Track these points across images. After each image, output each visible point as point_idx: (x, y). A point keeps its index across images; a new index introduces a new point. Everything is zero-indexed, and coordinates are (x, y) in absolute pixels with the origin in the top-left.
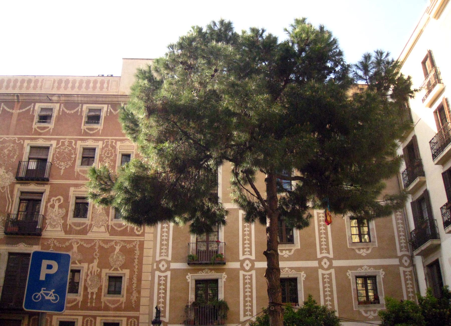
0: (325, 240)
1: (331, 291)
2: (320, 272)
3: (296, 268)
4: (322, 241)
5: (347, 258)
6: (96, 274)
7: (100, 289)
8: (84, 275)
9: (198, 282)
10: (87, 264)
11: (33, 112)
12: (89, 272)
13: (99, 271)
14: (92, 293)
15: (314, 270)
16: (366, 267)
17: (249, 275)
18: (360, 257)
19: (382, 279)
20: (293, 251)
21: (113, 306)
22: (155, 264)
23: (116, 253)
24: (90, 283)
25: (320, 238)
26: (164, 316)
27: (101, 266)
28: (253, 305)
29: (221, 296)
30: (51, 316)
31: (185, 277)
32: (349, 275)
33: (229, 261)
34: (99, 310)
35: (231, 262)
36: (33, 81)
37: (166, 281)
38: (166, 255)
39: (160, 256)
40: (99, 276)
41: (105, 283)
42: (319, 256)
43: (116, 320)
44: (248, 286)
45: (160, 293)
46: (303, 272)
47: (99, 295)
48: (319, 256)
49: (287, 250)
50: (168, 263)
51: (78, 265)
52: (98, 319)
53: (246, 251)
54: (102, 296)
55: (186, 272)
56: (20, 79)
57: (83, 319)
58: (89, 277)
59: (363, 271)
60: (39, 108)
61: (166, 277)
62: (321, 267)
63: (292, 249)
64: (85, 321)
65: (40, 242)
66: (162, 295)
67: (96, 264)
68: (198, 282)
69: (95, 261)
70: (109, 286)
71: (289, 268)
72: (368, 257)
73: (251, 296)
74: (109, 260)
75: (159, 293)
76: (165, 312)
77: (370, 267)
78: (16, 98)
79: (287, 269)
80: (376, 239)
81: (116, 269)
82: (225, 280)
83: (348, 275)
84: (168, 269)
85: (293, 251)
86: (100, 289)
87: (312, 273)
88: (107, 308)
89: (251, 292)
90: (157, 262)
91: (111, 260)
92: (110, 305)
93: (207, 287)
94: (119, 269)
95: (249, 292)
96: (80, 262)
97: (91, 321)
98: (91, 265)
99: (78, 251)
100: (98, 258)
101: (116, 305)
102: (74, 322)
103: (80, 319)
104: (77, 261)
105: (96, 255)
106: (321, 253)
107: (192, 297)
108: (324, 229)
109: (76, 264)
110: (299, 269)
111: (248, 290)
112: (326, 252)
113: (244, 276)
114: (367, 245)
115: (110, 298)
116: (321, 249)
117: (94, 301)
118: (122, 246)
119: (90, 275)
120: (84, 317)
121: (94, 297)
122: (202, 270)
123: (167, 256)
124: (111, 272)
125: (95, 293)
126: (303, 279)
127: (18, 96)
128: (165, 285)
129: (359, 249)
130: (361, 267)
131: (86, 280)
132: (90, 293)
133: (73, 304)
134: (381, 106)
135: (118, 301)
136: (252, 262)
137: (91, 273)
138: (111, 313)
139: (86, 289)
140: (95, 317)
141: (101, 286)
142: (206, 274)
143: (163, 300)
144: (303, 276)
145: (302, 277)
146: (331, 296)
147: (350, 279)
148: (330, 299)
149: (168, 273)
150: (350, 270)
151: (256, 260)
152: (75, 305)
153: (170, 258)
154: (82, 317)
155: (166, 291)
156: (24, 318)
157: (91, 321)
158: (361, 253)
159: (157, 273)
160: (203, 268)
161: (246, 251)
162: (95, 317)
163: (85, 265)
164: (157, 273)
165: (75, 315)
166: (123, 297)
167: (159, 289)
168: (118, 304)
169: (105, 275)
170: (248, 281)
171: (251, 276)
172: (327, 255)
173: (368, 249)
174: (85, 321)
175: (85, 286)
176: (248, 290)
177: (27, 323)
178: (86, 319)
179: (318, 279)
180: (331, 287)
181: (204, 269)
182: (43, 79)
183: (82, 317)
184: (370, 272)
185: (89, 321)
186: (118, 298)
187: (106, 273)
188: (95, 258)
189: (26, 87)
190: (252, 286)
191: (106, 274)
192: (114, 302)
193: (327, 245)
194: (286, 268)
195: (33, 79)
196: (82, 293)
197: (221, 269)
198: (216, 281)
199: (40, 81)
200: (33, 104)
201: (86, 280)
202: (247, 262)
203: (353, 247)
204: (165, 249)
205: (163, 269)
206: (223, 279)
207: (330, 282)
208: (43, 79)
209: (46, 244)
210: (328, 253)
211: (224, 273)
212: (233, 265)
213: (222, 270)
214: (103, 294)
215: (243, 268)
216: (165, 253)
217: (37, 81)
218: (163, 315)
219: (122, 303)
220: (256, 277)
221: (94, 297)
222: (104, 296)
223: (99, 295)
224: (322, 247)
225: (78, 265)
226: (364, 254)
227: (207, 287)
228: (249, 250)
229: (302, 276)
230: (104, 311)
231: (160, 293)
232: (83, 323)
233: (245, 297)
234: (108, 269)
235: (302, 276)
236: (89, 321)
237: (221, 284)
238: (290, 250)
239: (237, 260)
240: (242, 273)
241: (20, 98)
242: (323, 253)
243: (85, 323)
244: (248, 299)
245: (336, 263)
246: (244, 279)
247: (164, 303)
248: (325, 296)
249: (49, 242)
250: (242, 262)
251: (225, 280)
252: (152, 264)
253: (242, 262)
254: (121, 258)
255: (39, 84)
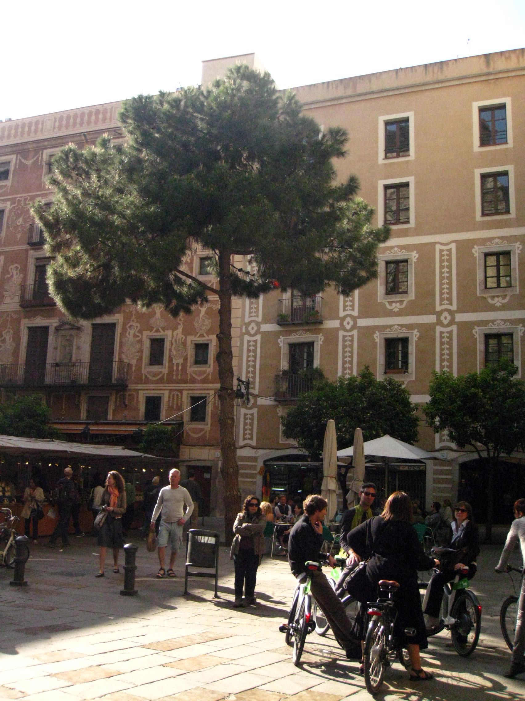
0: (448, 286)
1: (450, 355)
2: (438, 329)
3: (407, 324)
4: (444, 288)
5: (475, 311)
6: (180, 342)
7: (186, 359)
8: (168, 343)
9: (292, 346)
10: (171, 331)
11: (41, 162)
12: (174, 340)
13: (183, 339)
14: (178, 364)
15: (431, 327)
16: (499, 322)
17: (350, 336)
18: (494, 308)
19: (520, 339)
20: (405, 303)
21: (199, 378)
22: (244, 327)
23: (201, 315)
24: (174, 352)
25: (441, 284)
26: (254, 388)
27: (186, 332)
28: (354, 351)
29: (317, 363)
30: (137, 391)
31: (277, 341)
32: (476, 332)
33: (327, 319)
34: (185, 383)
35: (328, 320)
36: (101, 112)
37: (255, 346)
38: (255, 315)
39: (250, 316)
40: (184, 344)
41: (191, 352)
42: (438, 308)
43: (203, 393)
44: (348, 349)
45: (249, 361)
46: (416, 330)
47: (184, 365)
48: (438, 308)
49: (397, 302)
50: (258, 324)
51: (162, 333)
52: (185, 393)
53: (347, 306)
54: (188, 368)
55: (277, 334)
56: (87, 111)
57: (170, 393)
58: (174, 346)
59: (494, 327)
60: (47, 155)
61: (256, 341)
62: (439, 323)
63: (404, 301)
64: (171, 395)
65: (122, 309)
66: (251, 363)
67: (181, 330)
68: (292, 346)
69: (179, 327)
70: (197, 355)
71: (399, 325)
72: (504, 308)
73: (351, 362)
74: (194, 325)
75: (248, 361)
76: (254, 382)
77: (505, 321)
78: (83, 138)
79: (396, 327)
80: (518, 282)
81: (202, 336)
82: (322, 343)
83: (475, 333)
84: (258, 332)
85: (405, 303)
86: (186, 359)
87: (427, 331)
88: (193, 381)
89: (351, 357)
90: (246, 324)
91: (196, 325)
92: (196, 377)
93: (301, 353)
94: (205, 335)
95: (349, 357)
96: (164, 329)
97: (177, 395)
98: (175, 332)
99: (162, 317)
100: (183, 324)
101: (203, 377)
102: (160, 398)
103: (166, 393)
104: (160, 329)
105: (180, 320)
106: (441, 304)
107: (284, 365)
108: (447, 272)
109: (160, 332)
110: (410, 327)
111: (348, 354)
112: (448, 302)
113: (344, 337)
114: (504, 292)
115: (196, 369)
116: (442, 300)
117: (180, 373)
118: (208, 308)
119: (174, 344)
120: (171, 390)
121: (180, 368)
122: (296, 331)
123: (257, 316)
124: (196, 338)
125: (180, 364)
126: (415, 339)
127: (85, 135)
128: (255, 351)
129: (493, 297)
130: (493, 321)
131: (170, 350)
132: (175, 364)
133: (158, 377)
134: (277, 120)
135: (205, 372)
136: (354, 318)
137: (176, 341)
138: (198, 386)
139: (171, 360)
140: (181, 391)
141: (187, 355)
142: (301, 336)
143: (253, 370)
144: (416, 335)
145: (414, 336)
146: (450, 360)
147: (476, 338)
148: (448, 364)
149: (258, 337)
150: (478, 326)
151: (359, 317)
152: (160, 378)
153: (260, 319)
154: (168, 391)
155: (256, 358)
156: (111, 394)
157: (177, 395)
158: (493, 302)
159: (246, 338)
160: (298, 328)
161: (347, 306)
162: (181, 391)
163: (169, 333)
164: (246, 338)
165: (160, 390)
166: (210, 367)
167: (248, 356)
168: (205, 375)
169: (190, 342)
170: (348, 343)
171: (352, 336)
172: (449, 307)
173: (504, 297)
174: (171, 395)
175: (170, 356)
176: (348, 354)
177: (114, 400)
178: (172, 393)
179: (434, 340)
180: (450, 349)
181: (298, 330)
182: (112, 107)
183: (168, 391)
184: (504, 328)
185: (175, 396)
186: (204, 369)
187: (191, 339)
188: (180, 324)
189: (87, 123)
190: (352, 349)
191: (192, 341)
192: (200, 373)
193: (450, 293)
194: (394, 325)
195: (101, 109)
196: (167, 365)
197: (316, 329)
198: (311, 345)
199: (109, 110)
200: (41, 152)
201: (170, 350)
202: (348, 319)
203: (484, 295)
204: (255, 308)
205: (252, 332)
206: (319, 341)
207: (450, 343)
208: (112, 107)
209: (128, 311)
210: (451, 304)
211: (321, 334)
212: (331, 324)
213: (318, 331)
214: (188, 364)
215: (342, 327)
216: (255, 312)
217: (105, 111)
218: (252, 386)
219: (209, 374)
220: (359, 339)
221: (180, 368)
222: (190, 366)
223: (184, 365)
224: (443, 296)
225: (162, 333)
226: (499, 304)
227: (301, 353)
228: (351, 304)
229: (414, 335)
230: (190, 383)
231: (249, 361)
232: (169, 397)
233: (344, 363)
234: (193, 336)
235: (414, 335)
236: (175, 396)
237: (317, 348)
238: (401, 302)
239: (337, 317)
240: (341, 333)
241: (88, 137)
242: (444, 304)
243: (171, 397)
244: (348, 365)
245: (460, 317)
246: (344, 341)
247: (254, 372)
248: (442, 360)
249: (131, 309)
250: (343, 319)
251: (322, 343)
252: (241, 328)
253: (343, 319)
254: (207, 322)
255: (108, 115)
